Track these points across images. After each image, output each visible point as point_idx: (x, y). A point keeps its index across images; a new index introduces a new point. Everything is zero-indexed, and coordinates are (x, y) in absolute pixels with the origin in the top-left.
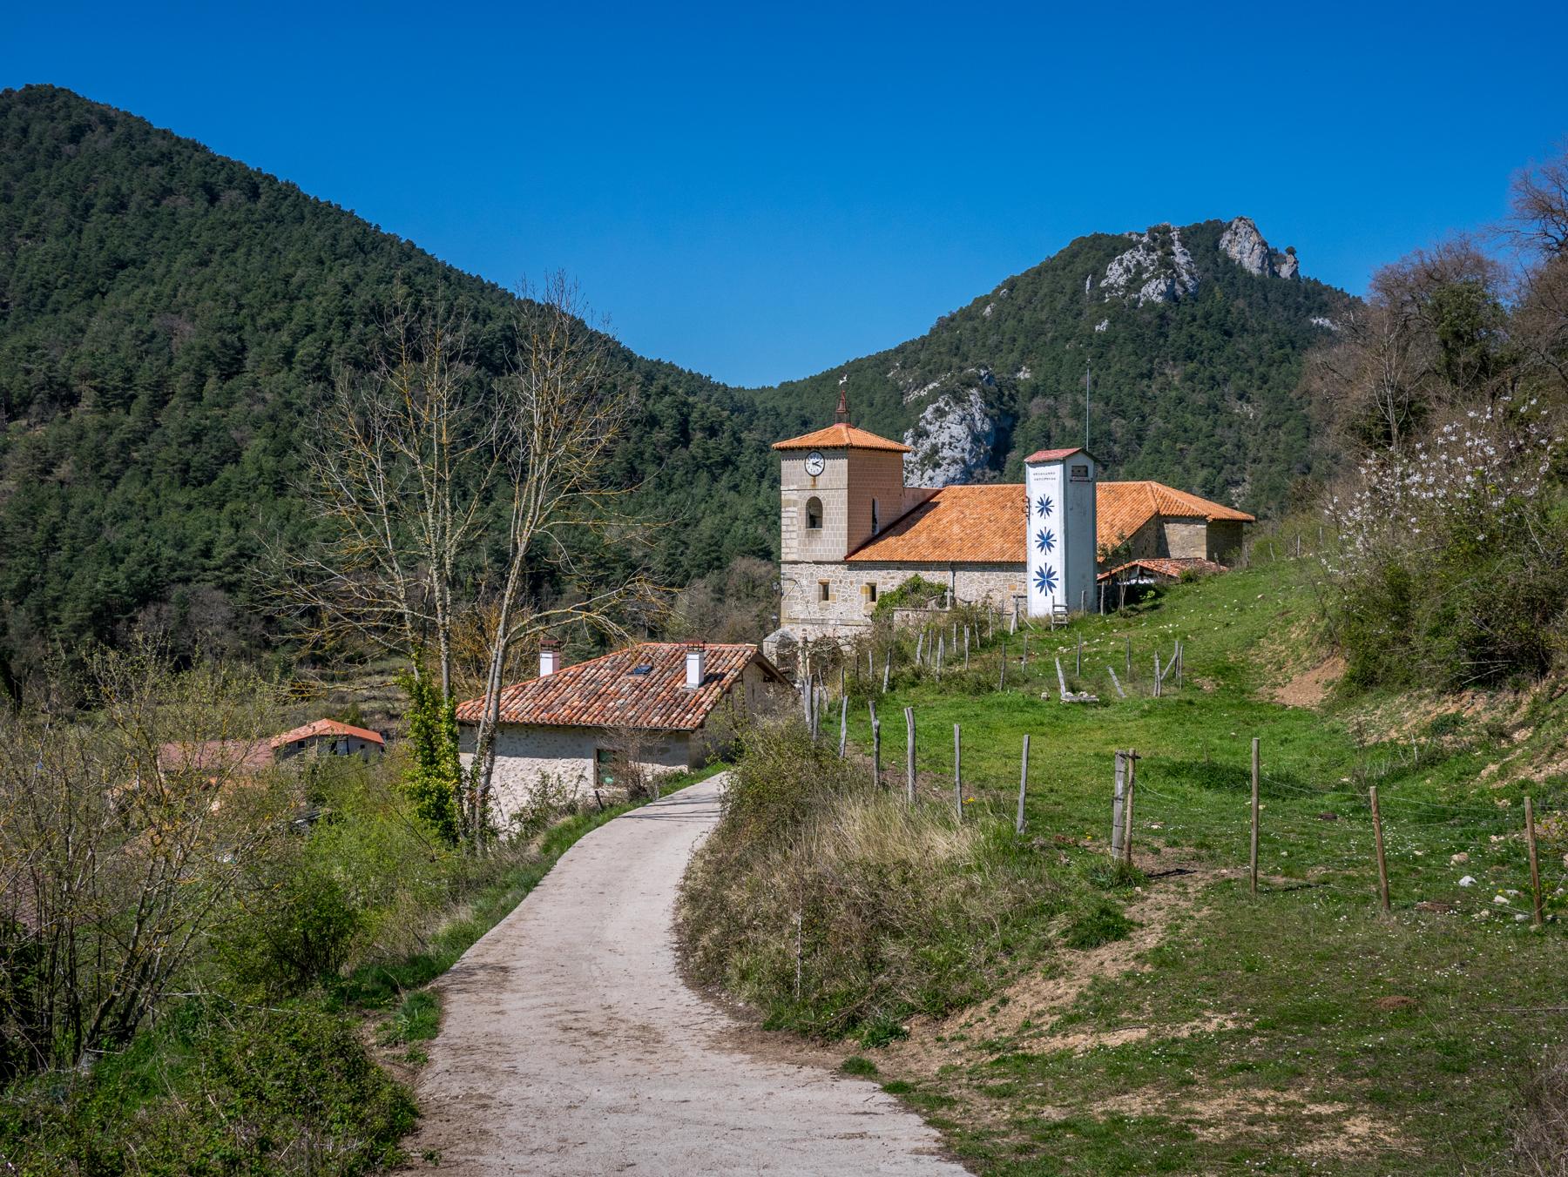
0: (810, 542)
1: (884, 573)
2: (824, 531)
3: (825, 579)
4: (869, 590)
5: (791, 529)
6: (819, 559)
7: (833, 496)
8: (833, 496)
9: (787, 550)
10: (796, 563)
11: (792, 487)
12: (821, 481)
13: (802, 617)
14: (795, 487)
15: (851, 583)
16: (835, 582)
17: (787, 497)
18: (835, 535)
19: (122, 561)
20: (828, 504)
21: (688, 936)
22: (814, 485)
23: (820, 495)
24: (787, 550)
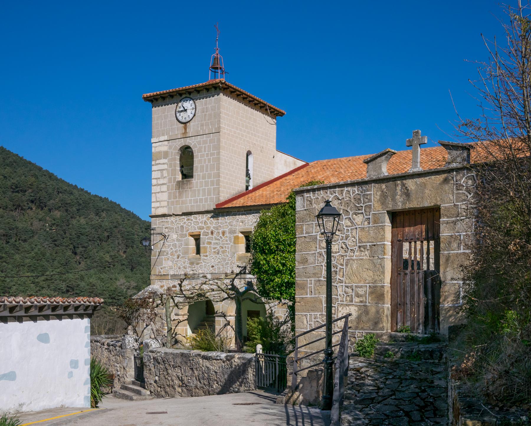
0: (180, 194)
1: (427, 178)
2: (194, 181)
3: (196, 231)
4: (202, 250)
5: (161, 181)
6: (190, 210)
7: (205, 142)
8: (205, 142)
9: (157, 204)
10: (164, 216)
11: (162, 138)
12: (192, 128)
13: (171, 273)
14: (166, 138)
15: (224, 233)
16: (206, 234)
17: (157, 150)
18: (206, 184)
19: (420, 379)
20: (200, 151)
21: (49, 337)
22: (185, 132)
23: (189, 142)
24: (157, 204)
